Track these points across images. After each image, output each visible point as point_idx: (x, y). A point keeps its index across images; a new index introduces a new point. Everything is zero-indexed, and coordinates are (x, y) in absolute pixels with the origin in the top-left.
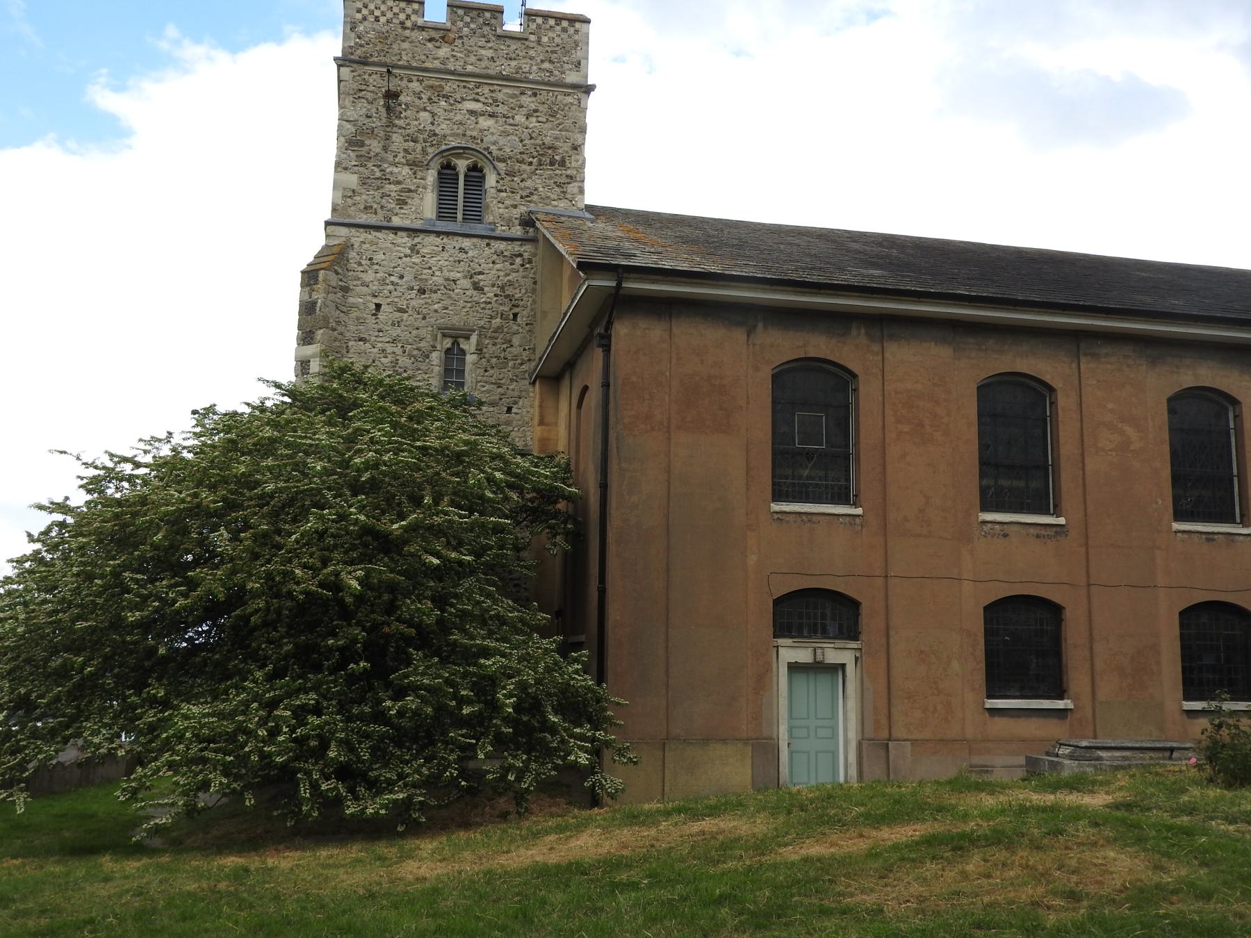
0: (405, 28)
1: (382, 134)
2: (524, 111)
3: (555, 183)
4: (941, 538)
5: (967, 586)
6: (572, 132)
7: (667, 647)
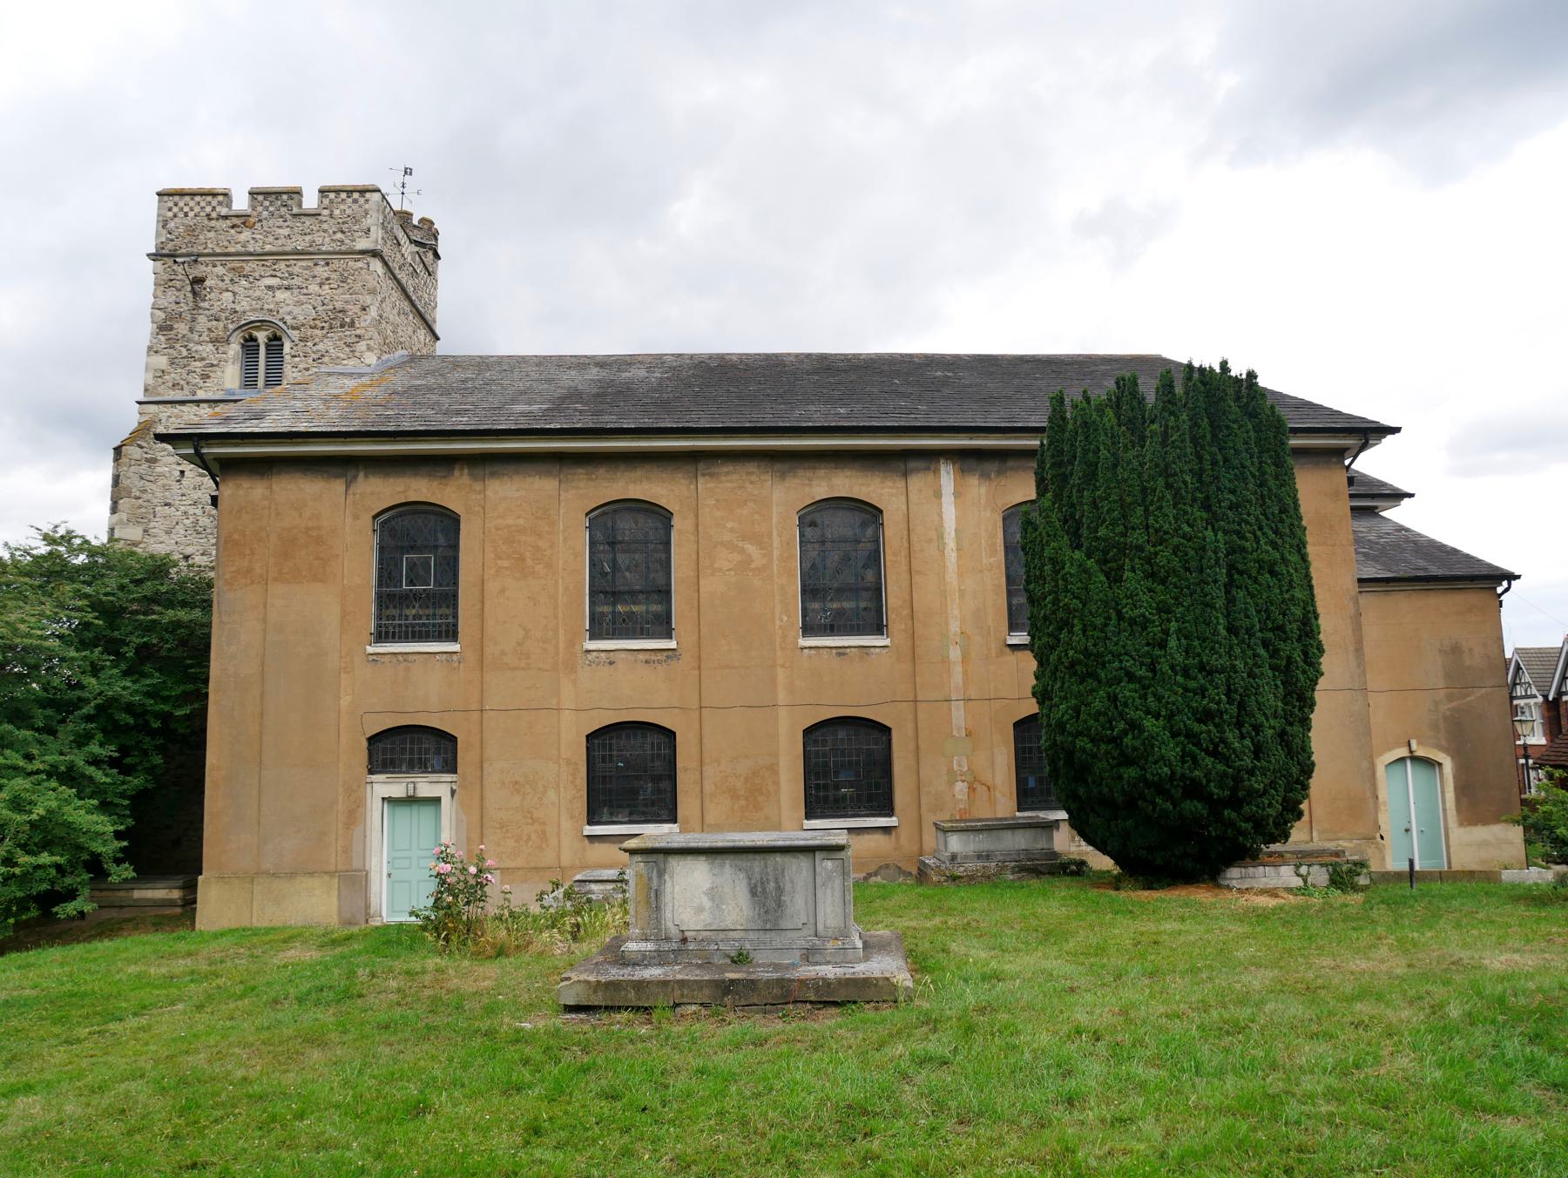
0: (210, 219)
1: (189, 317)
2: (318, 280)
3: (345, 343)
4: (540, 669)
5: (567, 717)
6: (362, 294)
7: (260, 786)
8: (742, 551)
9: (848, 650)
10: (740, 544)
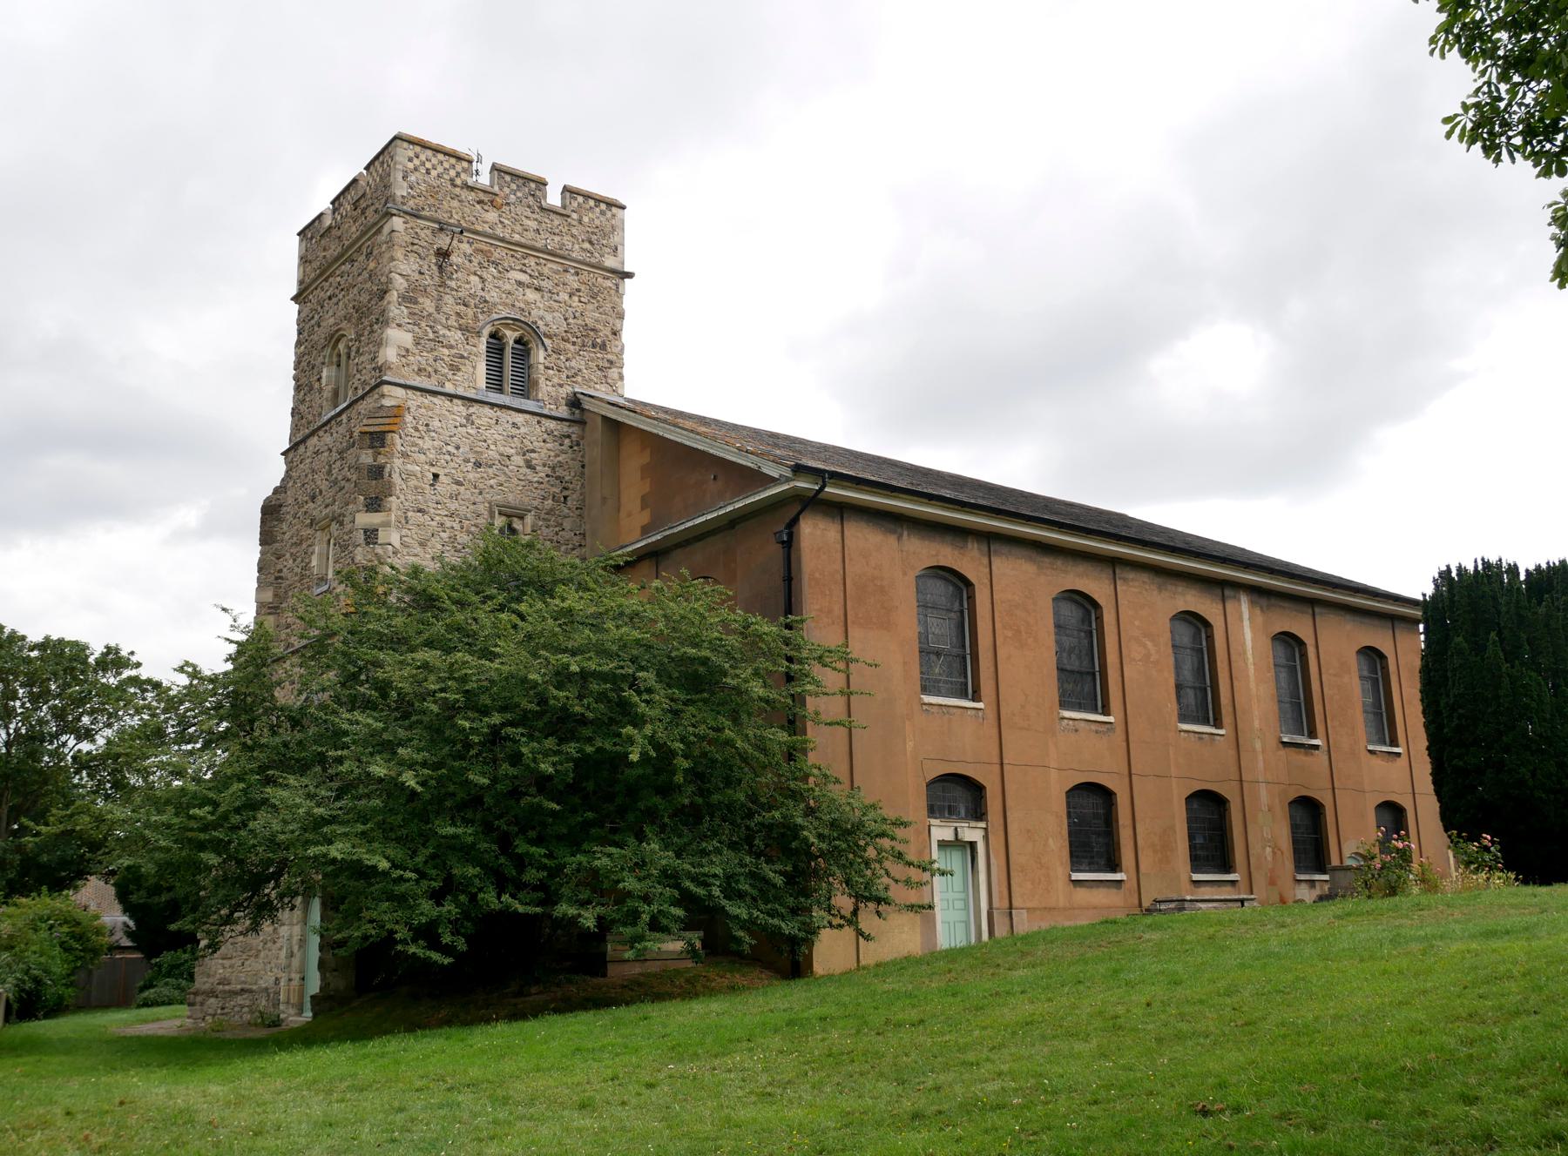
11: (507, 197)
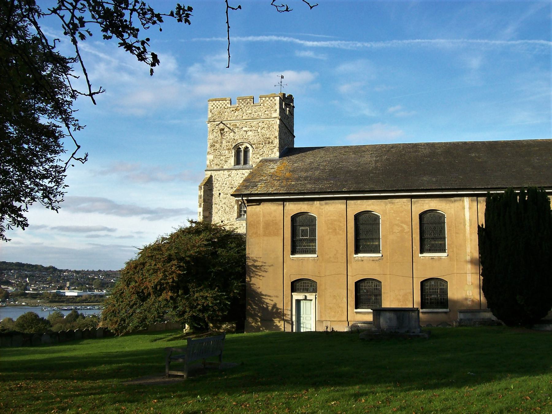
8: (402, 227)
9: (435, 257)
10: (401, 224)
11: (241, 106)
